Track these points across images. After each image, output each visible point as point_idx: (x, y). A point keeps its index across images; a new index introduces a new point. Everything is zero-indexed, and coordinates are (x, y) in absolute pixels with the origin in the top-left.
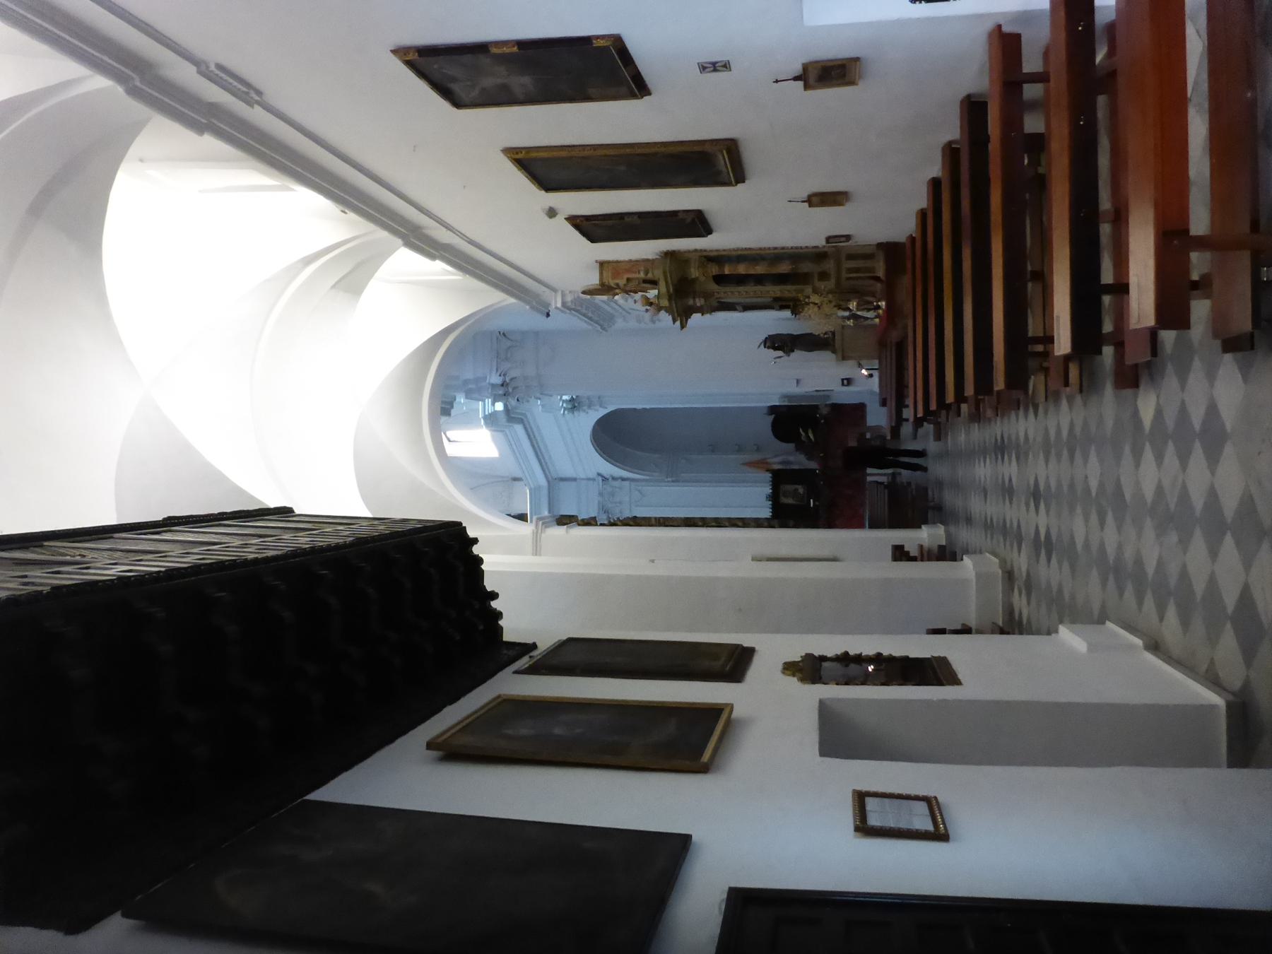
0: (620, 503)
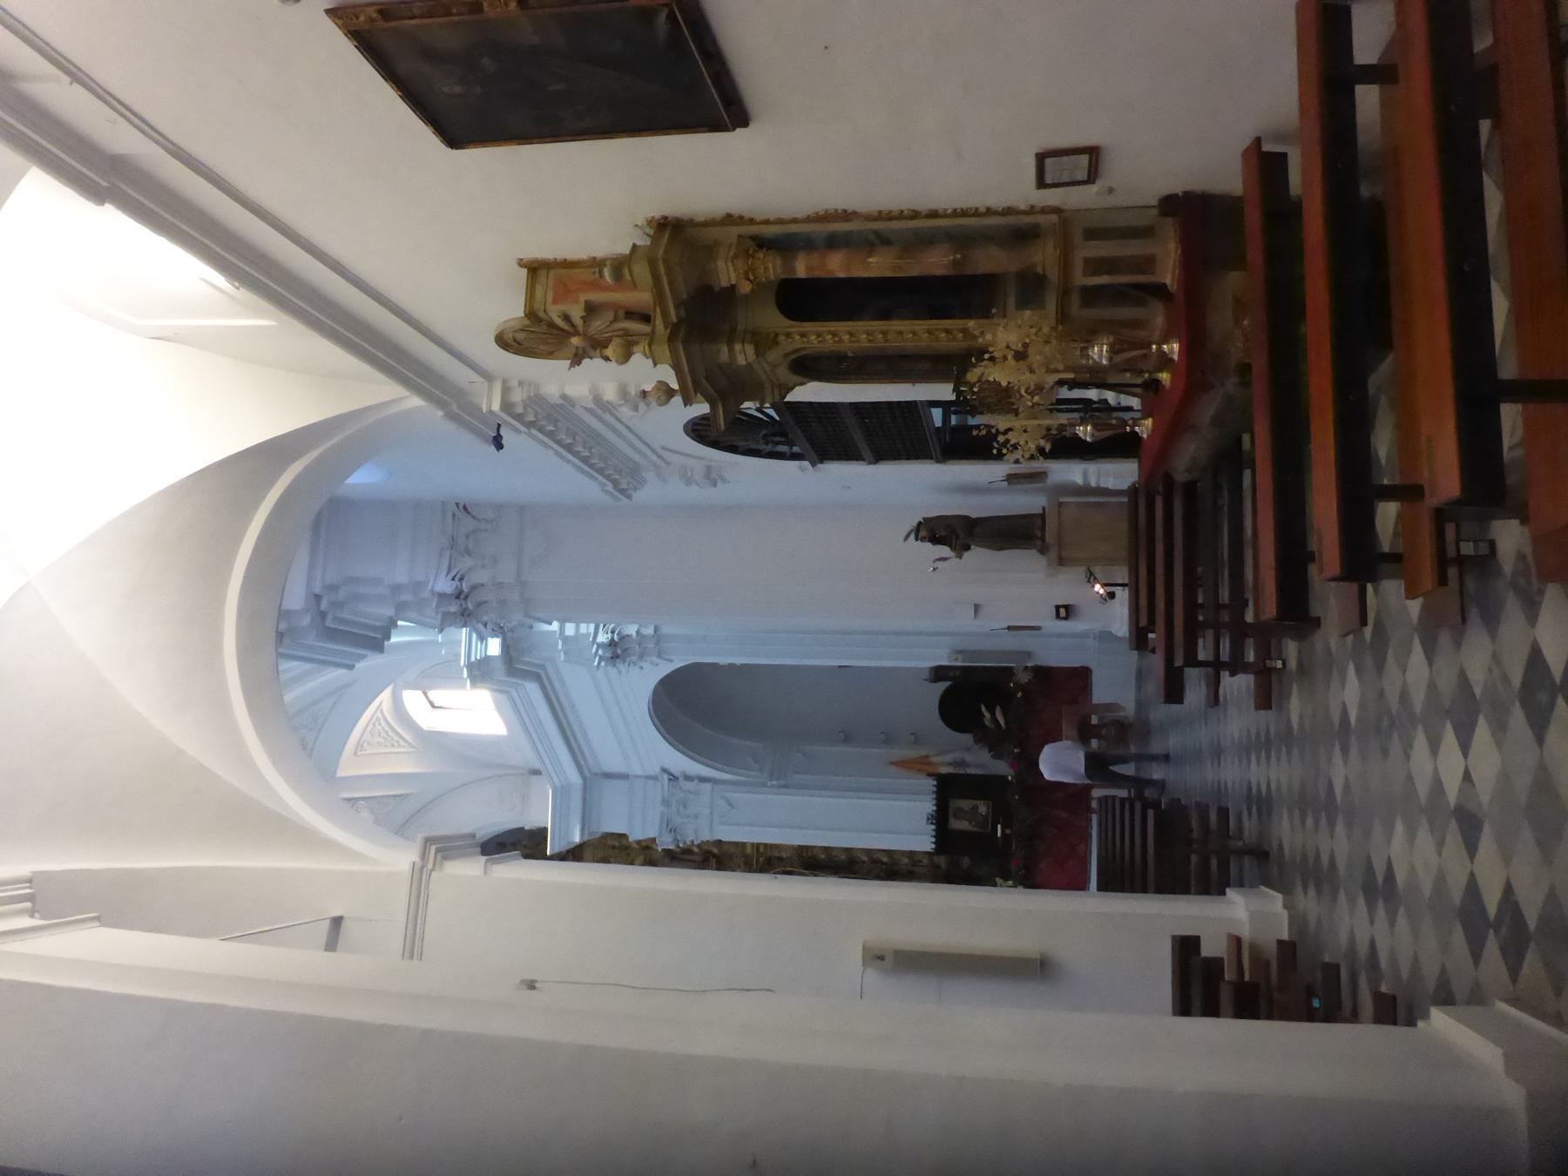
0: (696, 817)
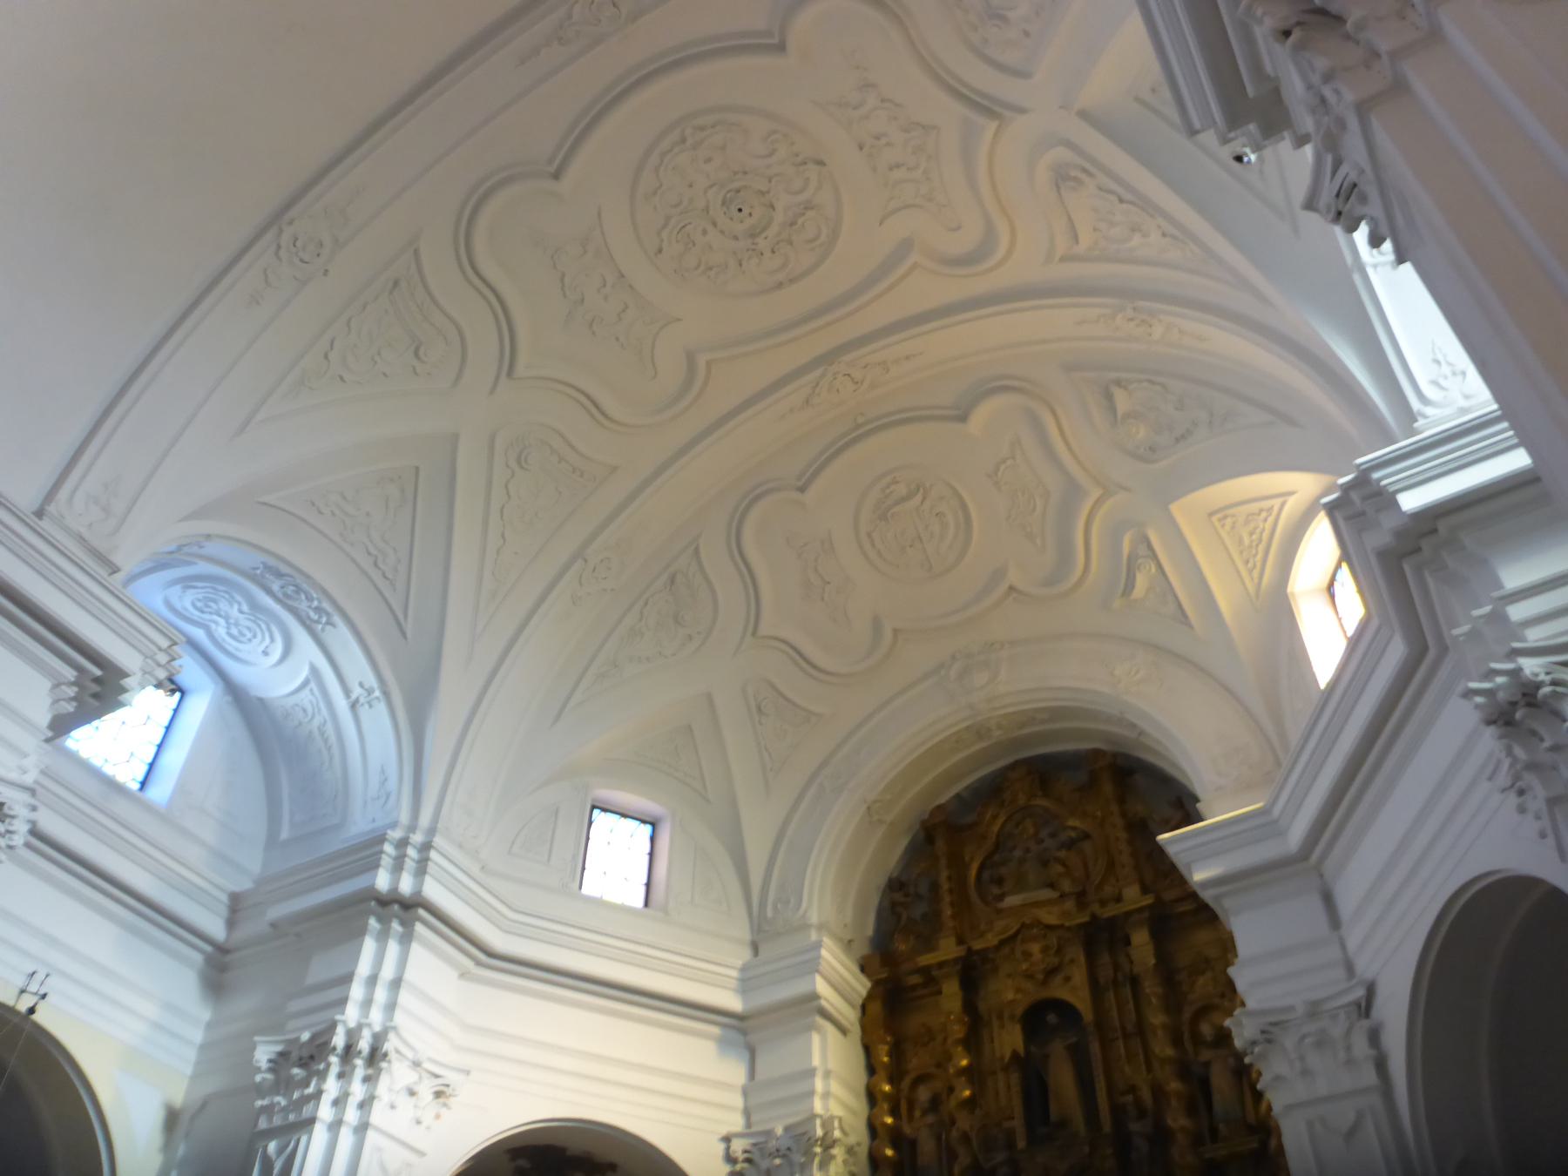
0: (1306, 1073)
